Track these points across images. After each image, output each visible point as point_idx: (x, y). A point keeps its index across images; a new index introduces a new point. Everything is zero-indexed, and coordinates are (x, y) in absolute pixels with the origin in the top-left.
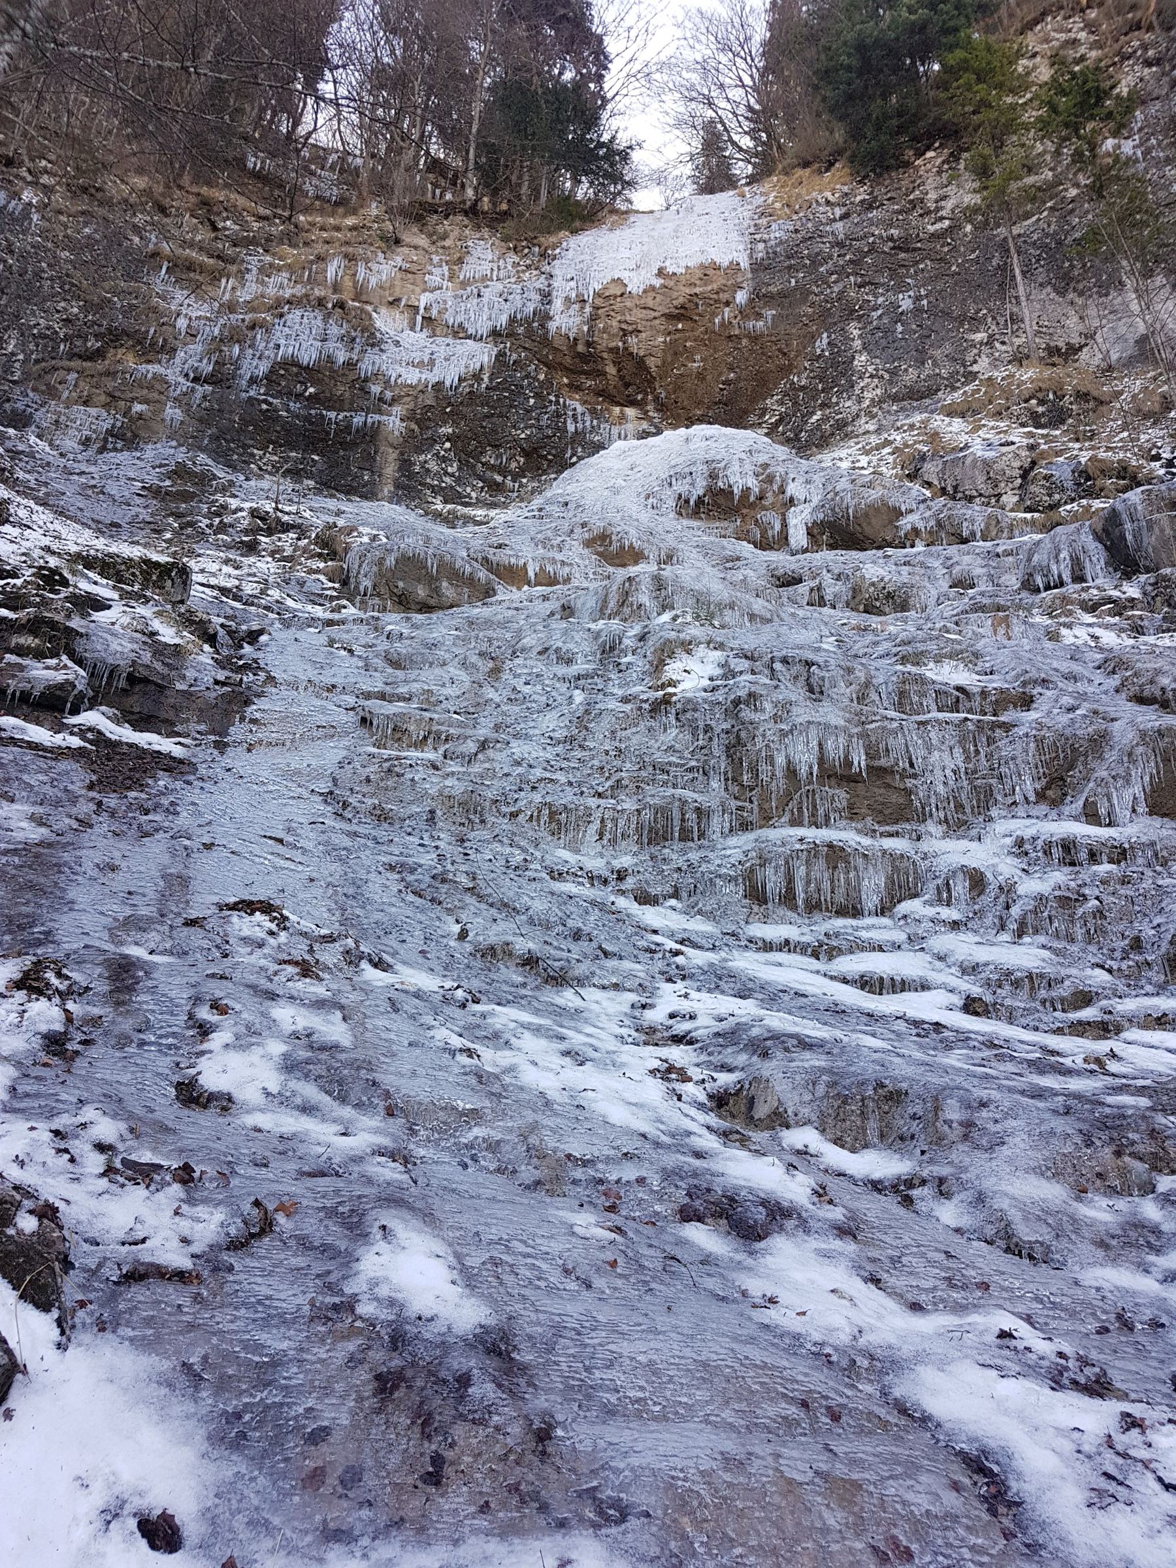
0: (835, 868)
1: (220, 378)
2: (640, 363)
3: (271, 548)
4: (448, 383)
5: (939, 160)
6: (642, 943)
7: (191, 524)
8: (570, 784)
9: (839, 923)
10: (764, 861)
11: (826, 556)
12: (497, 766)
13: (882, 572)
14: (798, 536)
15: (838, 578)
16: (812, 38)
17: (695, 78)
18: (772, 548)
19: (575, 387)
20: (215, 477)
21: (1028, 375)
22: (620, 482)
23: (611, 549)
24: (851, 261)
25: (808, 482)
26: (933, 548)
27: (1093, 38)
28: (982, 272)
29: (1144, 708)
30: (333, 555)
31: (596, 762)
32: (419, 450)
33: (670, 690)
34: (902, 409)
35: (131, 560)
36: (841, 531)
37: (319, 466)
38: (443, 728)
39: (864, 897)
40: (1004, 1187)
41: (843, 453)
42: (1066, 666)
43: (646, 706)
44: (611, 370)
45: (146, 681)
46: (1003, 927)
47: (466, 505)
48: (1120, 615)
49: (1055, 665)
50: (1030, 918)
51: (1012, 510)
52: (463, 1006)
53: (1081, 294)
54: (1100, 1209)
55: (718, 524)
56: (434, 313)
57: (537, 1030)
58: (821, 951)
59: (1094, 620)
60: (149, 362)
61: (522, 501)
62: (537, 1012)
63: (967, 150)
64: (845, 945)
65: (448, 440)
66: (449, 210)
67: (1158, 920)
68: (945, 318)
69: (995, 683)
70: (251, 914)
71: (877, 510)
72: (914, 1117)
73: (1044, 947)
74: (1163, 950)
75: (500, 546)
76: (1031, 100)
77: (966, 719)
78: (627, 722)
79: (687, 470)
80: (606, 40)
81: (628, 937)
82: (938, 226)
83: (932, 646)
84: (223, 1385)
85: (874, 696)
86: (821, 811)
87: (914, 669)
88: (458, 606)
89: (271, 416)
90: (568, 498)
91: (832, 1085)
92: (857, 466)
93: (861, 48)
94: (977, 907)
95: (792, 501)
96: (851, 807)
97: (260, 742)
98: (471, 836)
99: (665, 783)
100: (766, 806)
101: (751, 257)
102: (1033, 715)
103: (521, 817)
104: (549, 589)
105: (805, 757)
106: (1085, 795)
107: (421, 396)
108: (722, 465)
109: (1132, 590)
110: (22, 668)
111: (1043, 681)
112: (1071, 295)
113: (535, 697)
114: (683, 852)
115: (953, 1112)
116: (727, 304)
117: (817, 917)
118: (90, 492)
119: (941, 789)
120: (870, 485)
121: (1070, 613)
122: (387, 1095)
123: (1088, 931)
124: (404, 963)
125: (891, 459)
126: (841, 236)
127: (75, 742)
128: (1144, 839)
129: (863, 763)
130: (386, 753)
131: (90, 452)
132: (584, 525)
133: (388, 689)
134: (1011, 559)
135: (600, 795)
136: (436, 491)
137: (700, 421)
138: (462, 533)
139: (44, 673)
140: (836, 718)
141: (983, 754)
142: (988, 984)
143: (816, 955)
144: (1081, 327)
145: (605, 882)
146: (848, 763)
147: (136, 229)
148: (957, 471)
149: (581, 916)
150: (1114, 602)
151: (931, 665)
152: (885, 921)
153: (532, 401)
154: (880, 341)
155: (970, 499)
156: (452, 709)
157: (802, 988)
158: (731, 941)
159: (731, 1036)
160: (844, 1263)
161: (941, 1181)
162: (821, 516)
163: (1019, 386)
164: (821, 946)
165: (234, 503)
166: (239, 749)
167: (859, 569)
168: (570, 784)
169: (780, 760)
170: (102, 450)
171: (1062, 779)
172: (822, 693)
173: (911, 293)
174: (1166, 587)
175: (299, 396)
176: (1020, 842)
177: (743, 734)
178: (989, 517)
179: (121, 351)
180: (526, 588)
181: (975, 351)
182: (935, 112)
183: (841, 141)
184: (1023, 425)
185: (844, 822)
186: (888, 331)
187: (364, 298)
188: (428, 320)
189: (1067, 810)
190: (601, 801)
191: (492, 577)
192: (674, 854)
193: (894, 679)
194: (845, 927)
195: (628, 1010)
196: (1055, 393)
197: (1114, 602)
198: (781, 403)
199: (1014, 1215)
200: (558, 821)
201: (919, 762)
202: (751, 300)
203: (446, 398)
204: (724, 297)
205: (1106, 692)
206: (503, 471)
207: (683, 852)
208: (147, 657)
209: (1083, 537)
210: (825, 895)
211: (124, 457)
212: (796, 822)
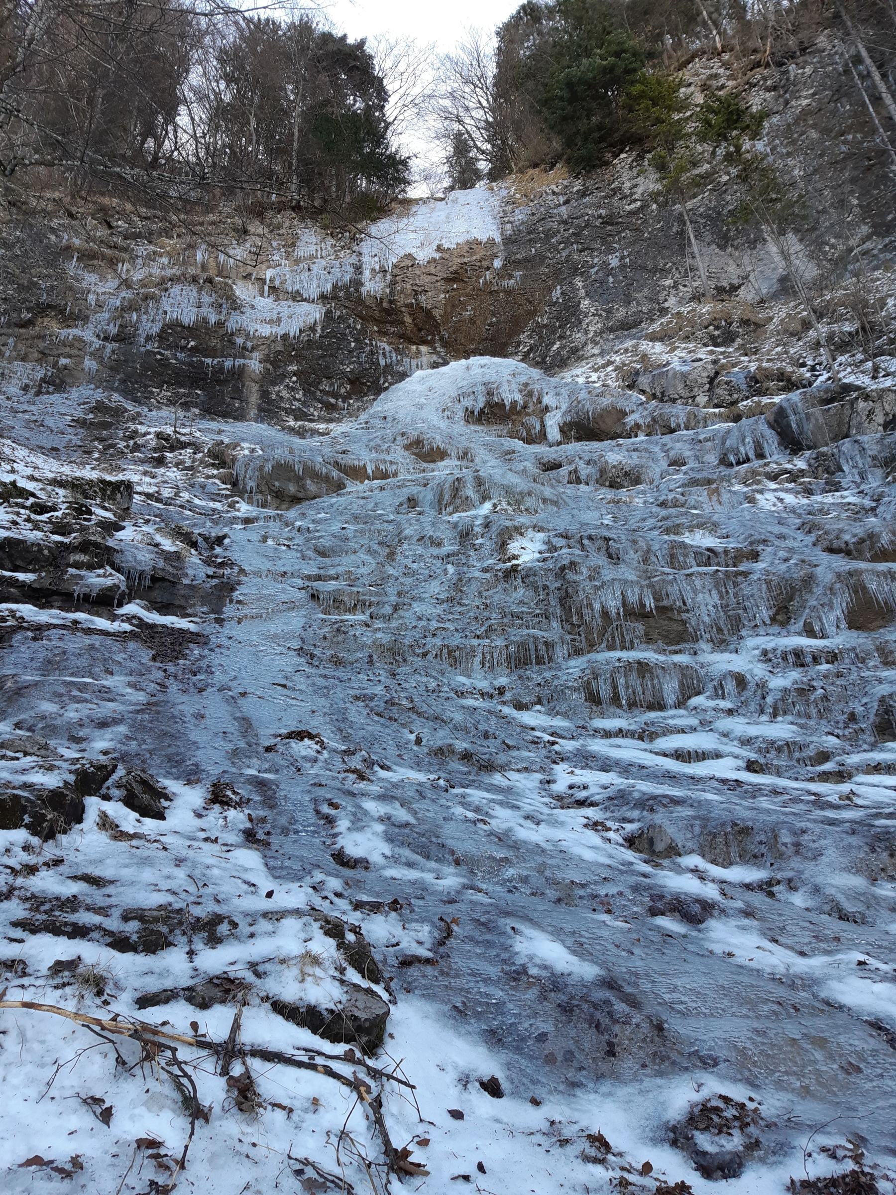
0: (644, 677)
1: (124, 337)
2: (428, 314)
3: (175, 461)
4: (292, 334)
5: (630, 160)
6: (528, 738)
7: (112, 446)
8: (457, 630)
9: (653, 715)
11: (574, 447)
12: (408, 622)
13: (619, 458)
14: (554, 434)
15: (588, 463)
16: (530, 75)
17: (447, 103)
18: (535, 442)
19: (382, 333)
20: (126, 410)
21: (705, 309)
22: (423, 400)
23: (425, 452)
24: (573, 234)
25: (557, 394)
27: (728, 72)
28: (667, 236)
29: (835, 556)
30: (223, 464)
31: (472, 614)
32: (274, 384)
33: (515, 562)
34: (617, 337)
35: (92, 481)
37: (202, 398)
38: (367, 598)
39: (665, 696)
40: (829, 881)
41: (578, 371)
42: (777, 529)
43: (500, 574)
44: (408, 319)
45: (163, 579)
46: (762, 712)
47: (311, 421)
48: (795, 481)
49: (770, 528)
50: (780, 703)
51: (704, 407)
52: (447, 791)
53: (736, 249)
54: (887, 890)
55: (495, 427)
56: (277, 283)
57: (501, 803)
58: (645, 735)
60: (68, 326)
61: (351, 416)
62: (488, 791)
63: (649, 152)
64: (660, 730)
65: (295, 375)
66: (280, 208)
67: (864, 700)
68: (642, 271)
70: (302, 740)
71: (609, 412)
72: (761, 843)
73: (792, 723)
74: (871, 720)
75: (344, 452)
76: (691, 116)
77: (718, 571)
80: (385, 82)
82: (633, 206)
83: (683, 520)
84: (478, 1015)
85: (654, 559)
86: (627, 639)
87: (676, 538)
88: (319, 497)
89: (164, 363)
91: (704, 827)
92: (588, 379)
93: (570, 85)
95: (547, 409)
97: (246, 616)
98: (399, 670)
99: (521, 626)
100: (590, 637)
101: (502, 234)
102: (761, 565)
104: (384, 482)
105: (613, 603)
107: (273, 345)
108: (495, 386)
109: (800, 464)
110: (81, 577)
111: (764, 541)
112: (730, 249)
113: (421, 571)
115: (786, 838)
116: (488, 269)
117: (636, 711)
118: (32, 425)
119: (707, 619)
120: (602, 395)
121: (759, 482)
122: (453, 853)
123: (819, 711)
125: (614, 374)
126: (565, 217)
127: (127, 627)
128: (848, 646)
130: (334, 618)
131: (30, 395)
132: (403, 434)
133: (322, 572)
134: (709, 443)
135: (478, 637)
136: (288, 412)
138: (312, 442)
139: (99, 579)
140: (631, 576)
142: (759, 751)
143: (641, 738)
144: (738, 272)
145: (491, 696)
146: (643, 606)
147: (53, 230)
150: (789, 472)
151: (687, 534)
152: (682, 712)
153: (353, 344)
155: (674, 401)
158: (583, 732)
159: (620, 798)
160: (755, 933)
161: (790, 881)
162: (569, 418)
163: (700, 317)
165: (142, 429)
166: (232, 622)
167: (602, 456)
168: (457, 630)
169: (597, 606)
170: (38, 393)
171: (786, 607)
172: (618, 558)
173: (617, 254)
174: (824, 460)
175: (183, 348)
176: (765, 653)
177: (570, 590)
179: (46, 320)
180: (366, 482)
182: (625, 127)
183: (560, 149)
184: (705, 345)
186: (603, 282)
187: (225, 274)
188: (273, 289)
189: (793, 628)
190: (480, 641)
191: (342, 475)
192: (534, 674)
195: (539, 785)
197: (789, 472)
198: (530, 337)
199: (841, 898)
200: (454, 657)
201: (689, 601)
202: (505, 265)
203: (292, 345)
204: (485, 264)
205: (806, 546)
206: (336, 395)
208: (161, 564)
209: (760, 426)
210: (640, 696)
211: (55, 398)
212: (611, 648)
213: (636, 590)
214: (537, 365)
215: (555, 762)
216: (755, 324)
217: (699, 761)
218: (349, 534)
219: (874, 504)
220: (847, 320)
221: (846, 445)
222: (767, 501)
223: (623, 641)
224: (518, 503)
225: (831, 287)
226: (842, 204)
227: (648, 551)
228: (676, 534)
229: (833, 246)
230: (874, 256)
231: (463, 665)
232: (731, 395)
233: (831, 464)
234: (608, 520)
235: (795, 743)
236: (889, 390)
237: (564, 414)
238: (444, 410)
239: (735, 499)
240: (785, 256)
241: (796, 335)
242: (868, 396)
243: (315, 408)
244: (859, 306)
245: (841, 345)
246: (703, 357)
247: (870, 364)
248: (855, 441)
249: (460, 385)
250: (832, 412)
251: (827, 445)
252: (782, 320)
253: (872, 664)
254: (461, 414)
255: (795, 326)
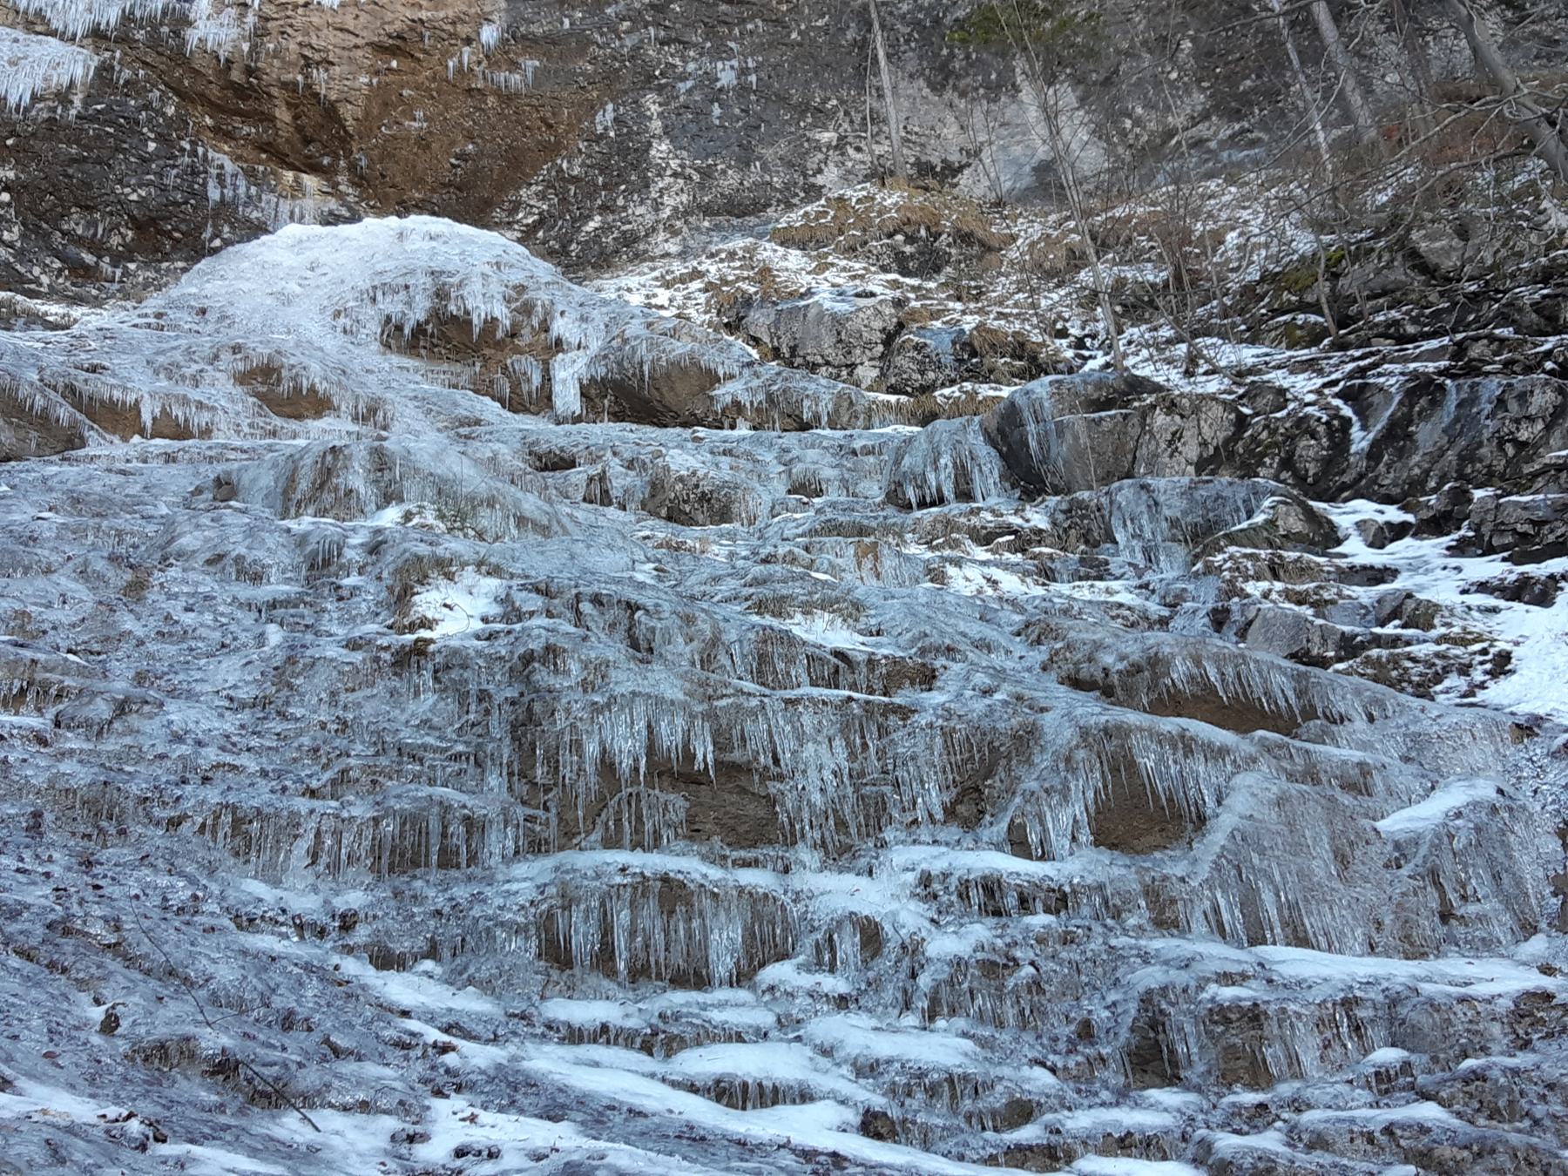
0: (671, 912)
2: (330, 112)
4: (12, 101)
6: (389, 1033)
8: (264, 774)
10: (568, 902)
11: (606, 431)
14: (567, 397)
18: (526, 411)
19: (223, 134)
23: (280, 392)
26: (764, 434)
28: (834, 46)
33: (424, 633)
36: (629, 395)
38: (54, 677)
39: (713, 957)
41: (632, 281)
42: (976, 630)
44: (283, 115)
46: (907, 1006)
47: (32, 294)
48: (1023, 551)
49: (962, 627)
50: (945, 992)
51: (870, 389)
52: (143, 1147)
53: (963, 94)
55: (445, 367)
58: (657, 1041)
59: (989, 556)
61: (127, 297)
62: (253, 1153)
64: (689, 1034)
67: (1112, 997)
69: (885, 649)
71: (684, 371)
73: (965, 1035)
74: (1122, 1039)
77: (850, 699)
78: (358, 679)
79: (401, 281)
81: (368, 1024)
83: (797, 589)
85: (724, 659)
86: (648, 826)
87: (775, 623)
88: (19, 459)
90: (206, 303)
92: (649, 302)
94: (871, 974)
95: (559, 345)
96: (691, 820)
99: (416, 777)
100: (569, 816)
102: (937, 698)
103: (186, 826)
104: (177, 444)
105: (627, 745)
106: (1010, 814)
109: (1037, 518)
111: (949, 649)
112: (949, 94)
113: (202, 631)
114: (445, 886)
116: (468, 41)
119: (817, 798)
120: (674, 333)
121: (956, 544)
123: (1022, 1012)
124: (30, 1075)
125: (702, 298)
128: (1090, 880)
129: (710, 757)
132: (236, 349)
134: (871, 459)
135: (313, 794)
137: (421, 207)
140: (673, 690)
141: (872, 750)
142: (892, 1091)
143: (647, 1048)
144: (962, 140)
145: (322, 933)
146: (690, 757)
148: (796, 326)
149: (292, 990)
150: (1015, 532)
151: (799, 617)
152: (743, 995)
153: (152, 146)
154: (689, 127)
155: (813, 368)
156: (63, 645)
157: (637, 1102)
158: (522, 1028)
162: (602, 371)
163: (880, 214)
164: (655, 1034)
167: (660, 455)
168: (264, 774)
169: (592, 748)
171: (977, 790)
172: (651, 650)
173: (735, 63)
174: (1083, 517)
176: (926, 880)
177: (537, 707)
178: (840, 396)
180: (136, 439)
181: (821, 156)
184: (885, 269)
185: (682, 844)
186: (701, 113)
189: (985, 834)
190: (316, 804)
191: (80, 417)
192: (431, 890)
193: (752, 636)
194: (688, 1004)
196: (928, 229)
197: (1015, 532)
198: (542, 196)
200: (245, 834)
202: (503, 41)
204: (464, 30)
205: (1029, 670)
206: (98, 248)
207: (445, 886)
209: (971, 437)
210: (657, 954)
212: (611, 843)
213: (680, 722)
214: (549, 255)
215: (439, 1093)
216: (982, 244)
217: (763, 1105)
218: (46, 531)
219: (1166, 612)
220: (1149, 260)
221: (1125, 492)
222: (965, 580)
223: (638, 830)
224: (461, 516)
225: (1126, 196)
226: (1163, 45)
227: (715, 642)
228: (778, 614)
229: (1137, 122)
230: (1210, 151)
231: (265, 857)
232: (922, 373)
233: (1094, 526)
234: (645, 573)
235: (965, 1078)
236: (1213, 397)
237: (593, 361)
238: (337, 314)
239: (906, 571)
240: (1050, 115)
241: (1058, 276)
242: (1173, 404)
243: (46, 268)
244: (1174, 238)
245: (1135, 306)
246: (877, 290)
247: (1183, 347)
248: (1143, 487)
249: (379, 267)
250: (1106, 426)
251: (1090, 488)
252: (1032, 245)
253: (1132, 921)
254: (374, 328)
255: (1056, 258)
